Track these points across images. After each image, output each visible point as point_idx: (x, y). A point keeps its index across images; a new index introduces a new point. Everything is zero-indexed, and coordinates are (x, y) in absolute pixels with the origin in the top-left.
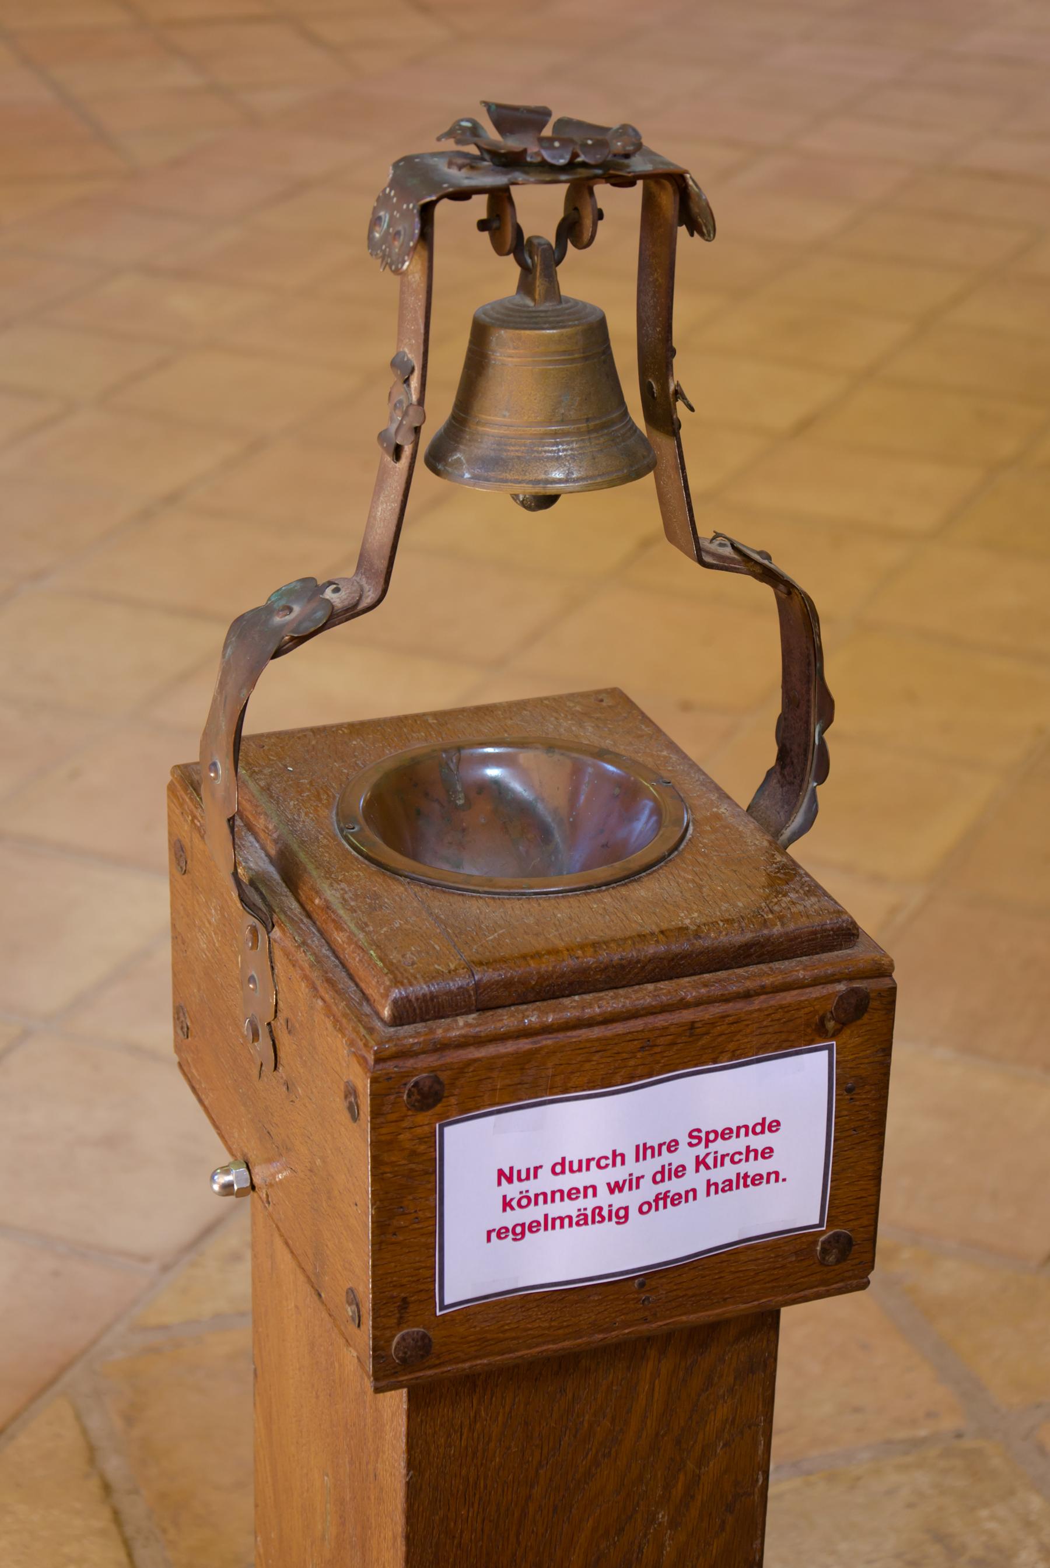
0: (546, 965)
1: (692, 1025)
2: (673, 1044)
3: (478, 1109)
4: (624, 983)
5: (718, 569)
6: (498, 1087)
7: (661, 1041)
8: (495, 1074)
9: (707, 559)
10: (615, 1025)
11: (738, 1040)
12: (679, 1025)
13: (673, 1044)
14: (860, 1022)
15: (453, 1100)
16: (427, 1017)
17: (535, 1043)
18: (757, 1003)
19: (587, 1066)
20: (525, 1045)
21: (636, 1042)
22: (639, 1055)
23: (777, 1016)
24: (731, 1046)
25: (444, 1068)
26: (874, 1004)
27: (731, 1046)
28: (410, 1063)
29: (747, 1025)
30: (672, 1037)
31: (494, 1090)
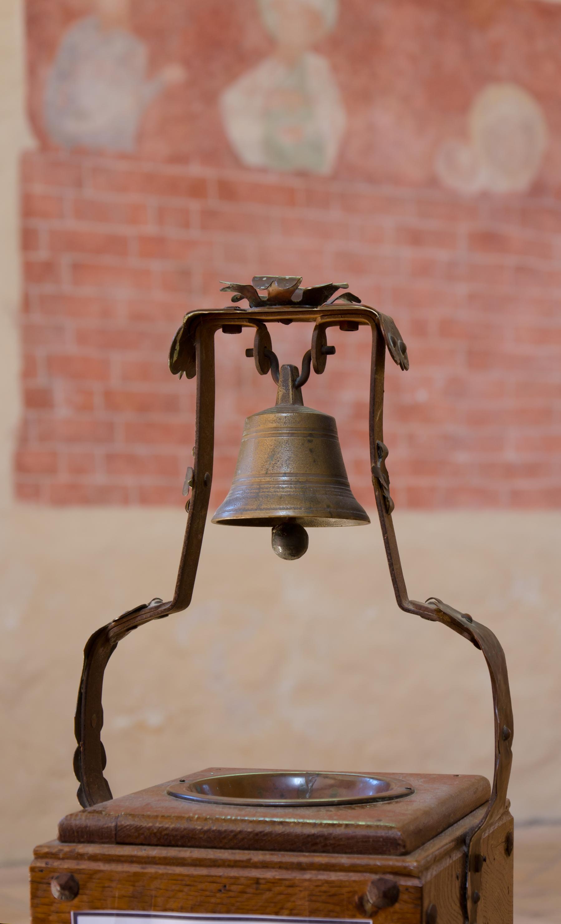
0: (169, 825)
1: (257, 881)
2: (243, 892)
3: (103, 908)
4: (221, 845)
5: (414, 614)
6: (117, 895)
7: (233, 888)
8: (114, 884)
9: (406, 605)
10: (202, 868)
11: (294, 902)
12: (247, 878)
13: (243, 892)
14: (391, 910)
15: (85, 898)
16: (82, 840)
17: (143, 868)
18: (308, 875)
19: (180, 895)
20: (135, 868)
21: (215, 885)
22: (218, 895)
23: (323, 888)
24: (289, 905)
25: (79, 871)
26: (404, 897)
27: (289, 905)
28: (56, 864)
29: (301, 891)
30: (243, 886)
31: (114, 897)
